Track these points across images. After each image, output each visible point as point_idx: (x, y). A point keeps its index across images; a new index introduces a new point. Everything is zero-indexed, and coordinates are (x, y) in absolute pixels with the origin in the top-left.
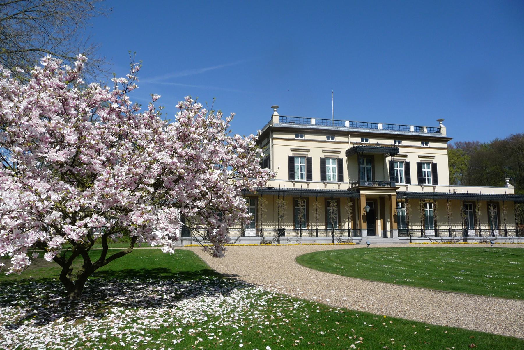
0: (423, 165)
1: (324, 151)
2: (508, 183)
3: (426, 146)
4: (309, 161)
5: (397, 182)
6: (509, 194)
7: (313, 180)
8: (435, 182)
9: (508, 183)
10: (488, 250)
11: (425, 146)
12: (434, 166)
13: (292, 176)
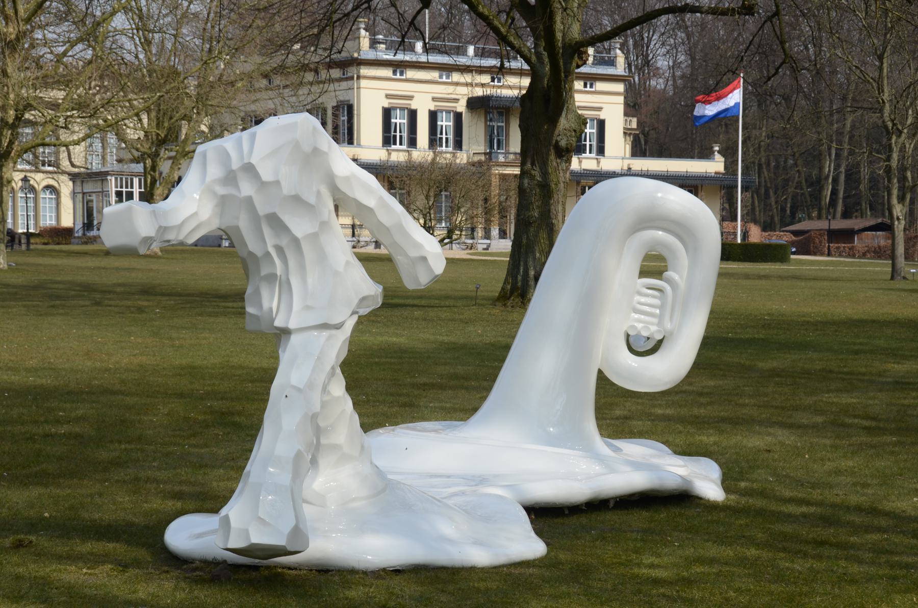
0: (392, 112)
1: (388, 96)
2: (716, 153)
3: (447, 80)
4: (413, 115)
5: (395, 144)
6: (716, 173)
7: (418, 147)
8: (601, 151)
9: (716, 153)
10: (118, 289)
11: (444, 79)
12: (601, 124)
13: (388, 140)
